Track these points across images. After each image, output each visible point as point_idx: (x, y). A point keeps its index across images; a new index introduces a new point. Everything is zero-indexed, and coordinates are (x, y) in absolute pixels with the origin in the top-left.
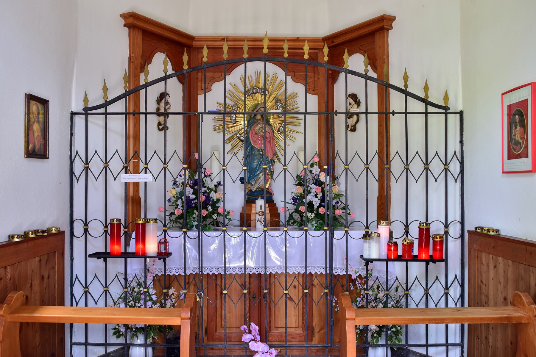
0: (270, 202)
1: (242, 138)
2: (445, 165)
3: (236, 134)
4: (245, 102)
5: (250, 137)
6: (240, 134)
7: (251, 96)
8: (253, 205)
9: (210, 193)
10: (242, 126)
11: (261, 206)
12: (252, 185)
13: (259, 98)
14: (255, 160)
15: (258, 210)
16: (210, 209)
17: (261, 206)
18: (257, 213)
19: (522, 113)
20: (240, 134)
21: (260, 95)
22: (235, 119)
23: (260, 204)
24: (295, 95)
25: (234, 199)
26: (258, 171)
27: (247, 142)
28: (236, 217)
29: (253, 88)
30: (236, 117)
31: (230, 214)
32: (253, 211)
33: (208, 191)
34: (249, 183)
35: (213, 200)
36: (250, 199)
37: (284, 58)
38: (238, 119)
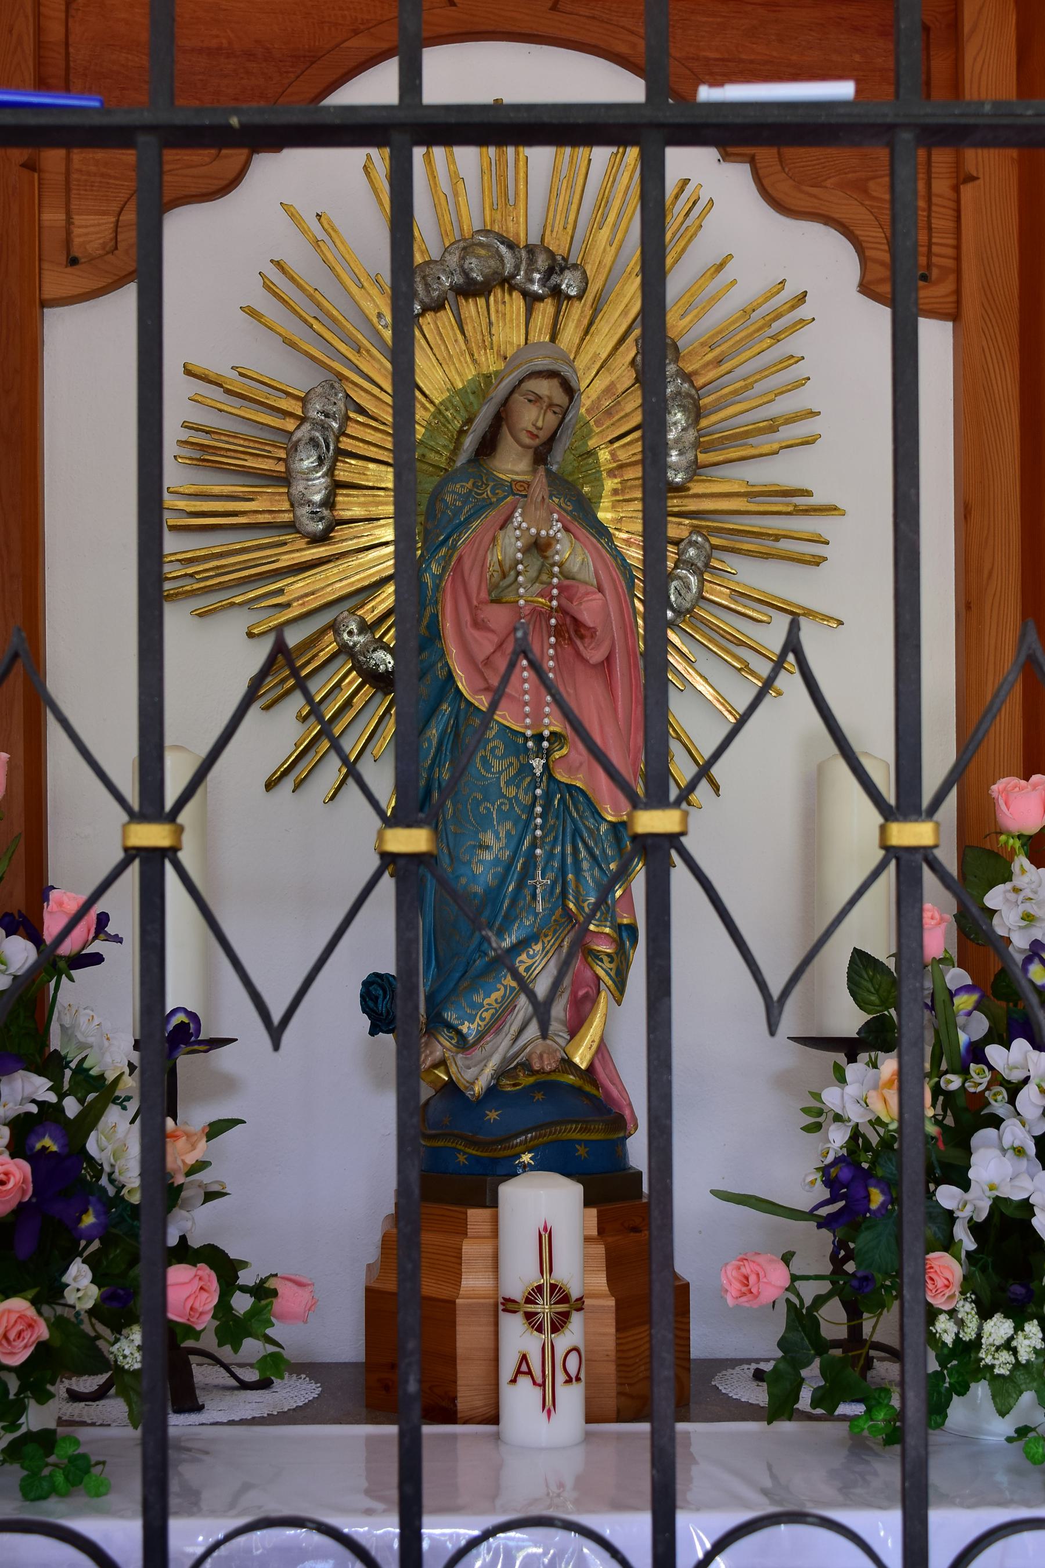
0: (629, 1211)
1: (385, 660)
2: (888, 813)
3: (334, 627)
4: (402, 357)
5: (448, 627)
6: (365, 628)
7: (446, 317)
8: (476, 1216)
9: (90, 1119)
10: (382, 561)
11: (545, 1238)
12: (463, 1043)
13: (507, 326)
14: (484, 822)
15: (520, 1273)
16: (80, 1283)
17: (545, 1238)
18: (509, 1305)
19: (483, 766)
20: (365, 628)
21: (518, 303)
22: (329, 503)
23: (542, 1212)
24: (781, 314)
25: (296, 1162)
26: (509, 920)
27: (413, 680)
28: (330, 1325)
29: (468, 248)
30: (338, 485)
31: (278, 1305)
32: (474, 1282)
33: (72, 1107)
34: (436, 1022)
35: (119, 1199)
36: (449, 1165)
37: (135, 1373)
38: (350, 506)
